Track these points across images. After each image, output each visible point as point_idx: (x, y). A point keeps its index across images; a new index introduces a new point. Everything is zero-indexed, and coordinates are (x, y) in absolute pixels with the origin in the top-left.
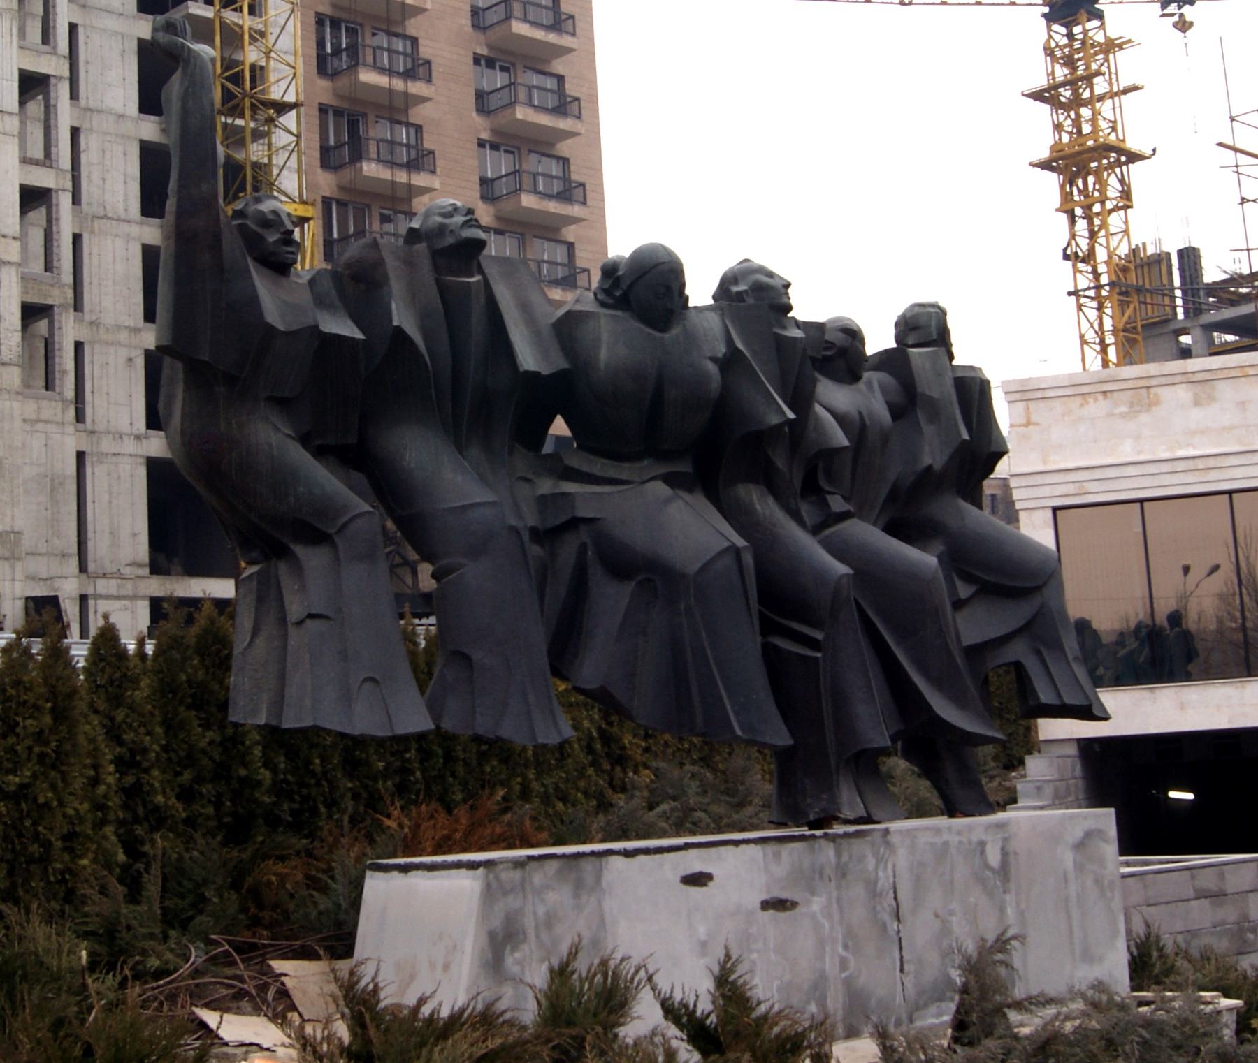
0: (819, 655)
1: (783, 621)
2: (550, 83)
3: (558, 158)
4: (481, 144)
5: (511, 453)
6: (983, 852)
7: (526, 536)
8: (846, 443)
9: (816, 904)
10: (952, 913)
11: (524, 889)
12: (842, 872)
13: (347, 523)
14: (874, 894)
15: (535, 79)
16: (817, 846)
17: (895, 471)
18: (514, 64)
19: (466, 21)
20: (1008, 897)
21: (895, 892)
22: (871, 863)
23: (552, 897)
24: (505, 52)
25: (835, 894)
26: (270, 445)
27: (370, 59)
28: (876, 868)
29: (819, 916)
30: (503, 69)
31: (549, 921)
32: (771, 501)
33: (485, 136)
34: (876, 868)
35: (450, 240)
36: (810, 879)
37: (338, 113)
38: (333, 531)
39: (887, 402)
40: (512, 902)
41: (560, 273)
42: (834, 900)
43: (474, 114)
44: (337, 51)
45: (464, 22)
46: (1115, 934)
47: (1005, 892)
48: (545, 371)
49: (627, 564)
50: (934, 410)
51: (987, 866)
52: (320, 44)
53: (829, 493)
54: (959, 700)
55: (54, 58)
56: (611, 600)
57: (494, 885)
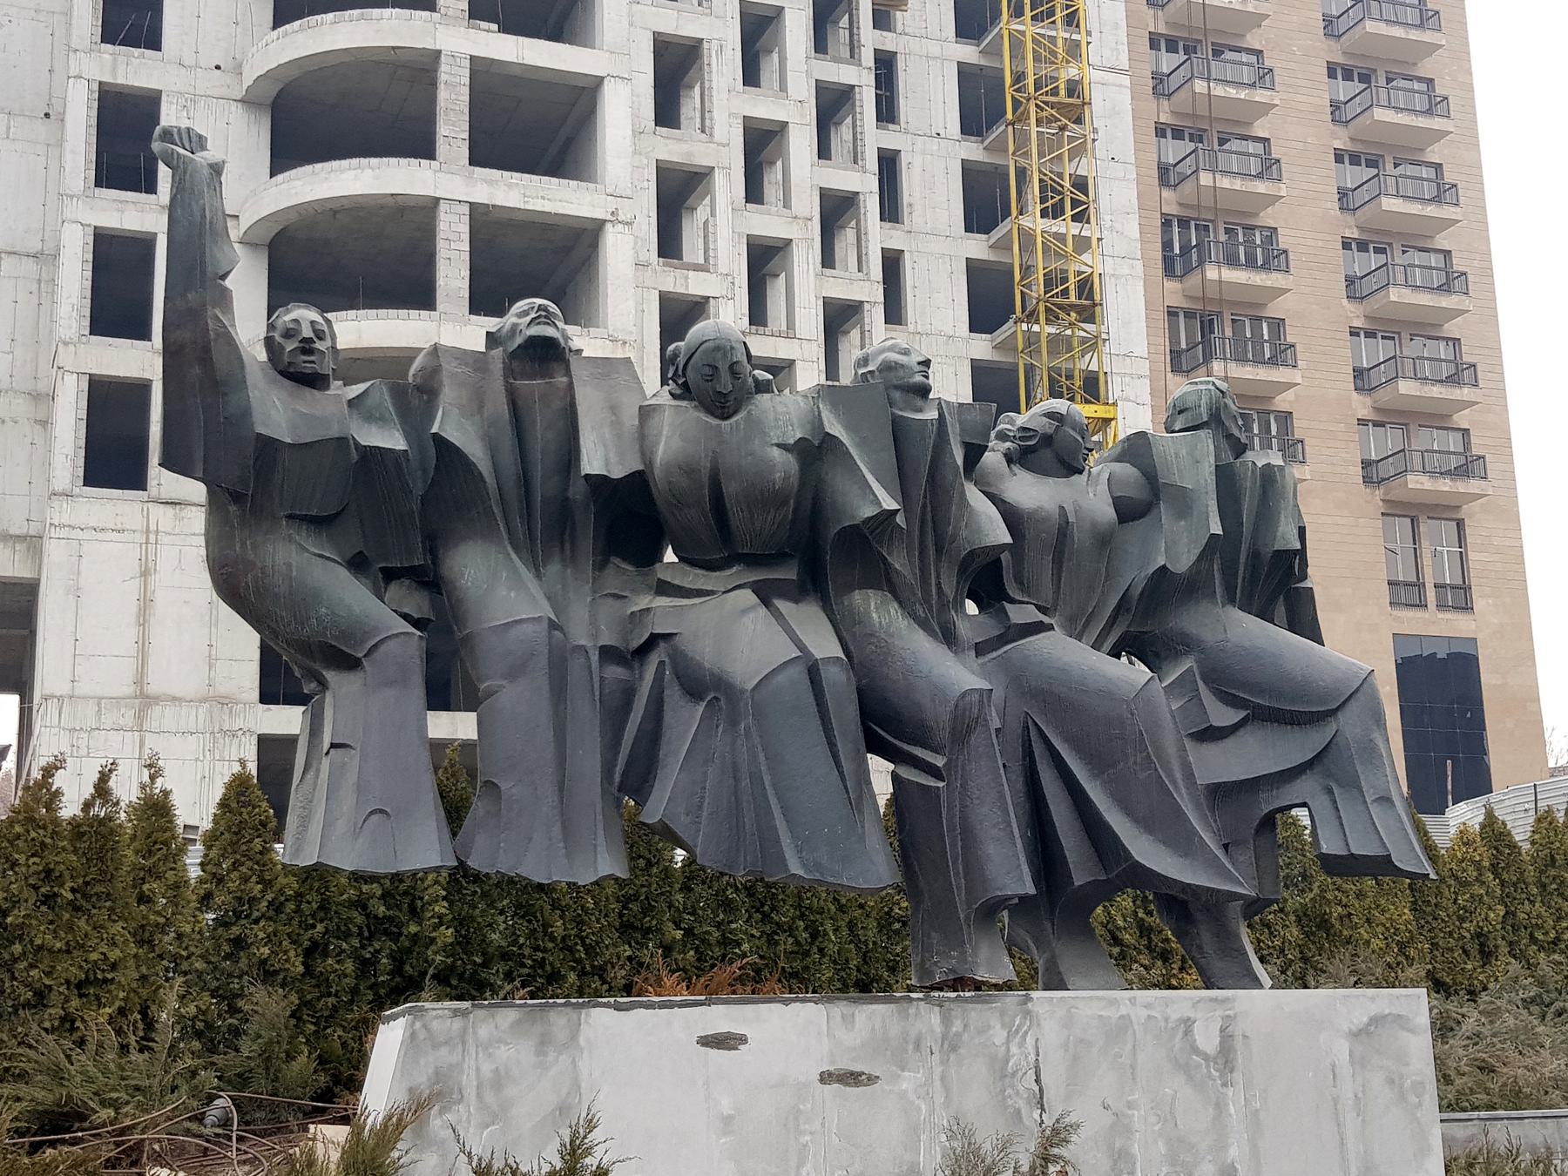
0: (941, 784)
1: (906, 747)
2: (1435, 260)
3: (1447, 339)
4: (1354, 333)
5: (601, 566)
6: (1188, 1032)
7: (595, 657)
8: (1008, 539)
9: (909, 1082)
10: (1130, 1105)
11: (464, 1043)
12: (951, 1045)
13: (376, 646)
14: (1002, 1072)
15: (1417, 258)
16: (912, 1011)
17: (1134, 574)
18: (1390, 245)
19: (1333, 204)
20: (1230, 1092)
21: (1038, 1074)
22: (999, 1035)
23: (503, 1053)
24: (1377, 232)
25: (938, 1070)
26: (289, 565)
27: (1400, 278)
28: (1008, 1042)
29: (912, 1097)
30: (1377, 250)
31: (499, 1081)
32: (894, 607)
33: (1357, 323)
34: (1008, 1042)
35: (519, 340)
36: (903, 1052)
37: (1189, 315)
38: (360, 655)
39: (1114, 499)
40: (445, 1056)
41: (1454, 462)
42: (936, 1077)
43: (1345, 301)
44: (1186, 249)
45: (1329, 205)
46: (1424, 1151)
47: (1224, 1085)
48: (617, 473)
49: (700, 685)
50: (1184, 502)
51: (1195, 1050)
52: (1167, 245)
53: (1013, 601)
54: (1181, 840)
55: (867, 284)
56: (685, 721)
57: (422, 1035)
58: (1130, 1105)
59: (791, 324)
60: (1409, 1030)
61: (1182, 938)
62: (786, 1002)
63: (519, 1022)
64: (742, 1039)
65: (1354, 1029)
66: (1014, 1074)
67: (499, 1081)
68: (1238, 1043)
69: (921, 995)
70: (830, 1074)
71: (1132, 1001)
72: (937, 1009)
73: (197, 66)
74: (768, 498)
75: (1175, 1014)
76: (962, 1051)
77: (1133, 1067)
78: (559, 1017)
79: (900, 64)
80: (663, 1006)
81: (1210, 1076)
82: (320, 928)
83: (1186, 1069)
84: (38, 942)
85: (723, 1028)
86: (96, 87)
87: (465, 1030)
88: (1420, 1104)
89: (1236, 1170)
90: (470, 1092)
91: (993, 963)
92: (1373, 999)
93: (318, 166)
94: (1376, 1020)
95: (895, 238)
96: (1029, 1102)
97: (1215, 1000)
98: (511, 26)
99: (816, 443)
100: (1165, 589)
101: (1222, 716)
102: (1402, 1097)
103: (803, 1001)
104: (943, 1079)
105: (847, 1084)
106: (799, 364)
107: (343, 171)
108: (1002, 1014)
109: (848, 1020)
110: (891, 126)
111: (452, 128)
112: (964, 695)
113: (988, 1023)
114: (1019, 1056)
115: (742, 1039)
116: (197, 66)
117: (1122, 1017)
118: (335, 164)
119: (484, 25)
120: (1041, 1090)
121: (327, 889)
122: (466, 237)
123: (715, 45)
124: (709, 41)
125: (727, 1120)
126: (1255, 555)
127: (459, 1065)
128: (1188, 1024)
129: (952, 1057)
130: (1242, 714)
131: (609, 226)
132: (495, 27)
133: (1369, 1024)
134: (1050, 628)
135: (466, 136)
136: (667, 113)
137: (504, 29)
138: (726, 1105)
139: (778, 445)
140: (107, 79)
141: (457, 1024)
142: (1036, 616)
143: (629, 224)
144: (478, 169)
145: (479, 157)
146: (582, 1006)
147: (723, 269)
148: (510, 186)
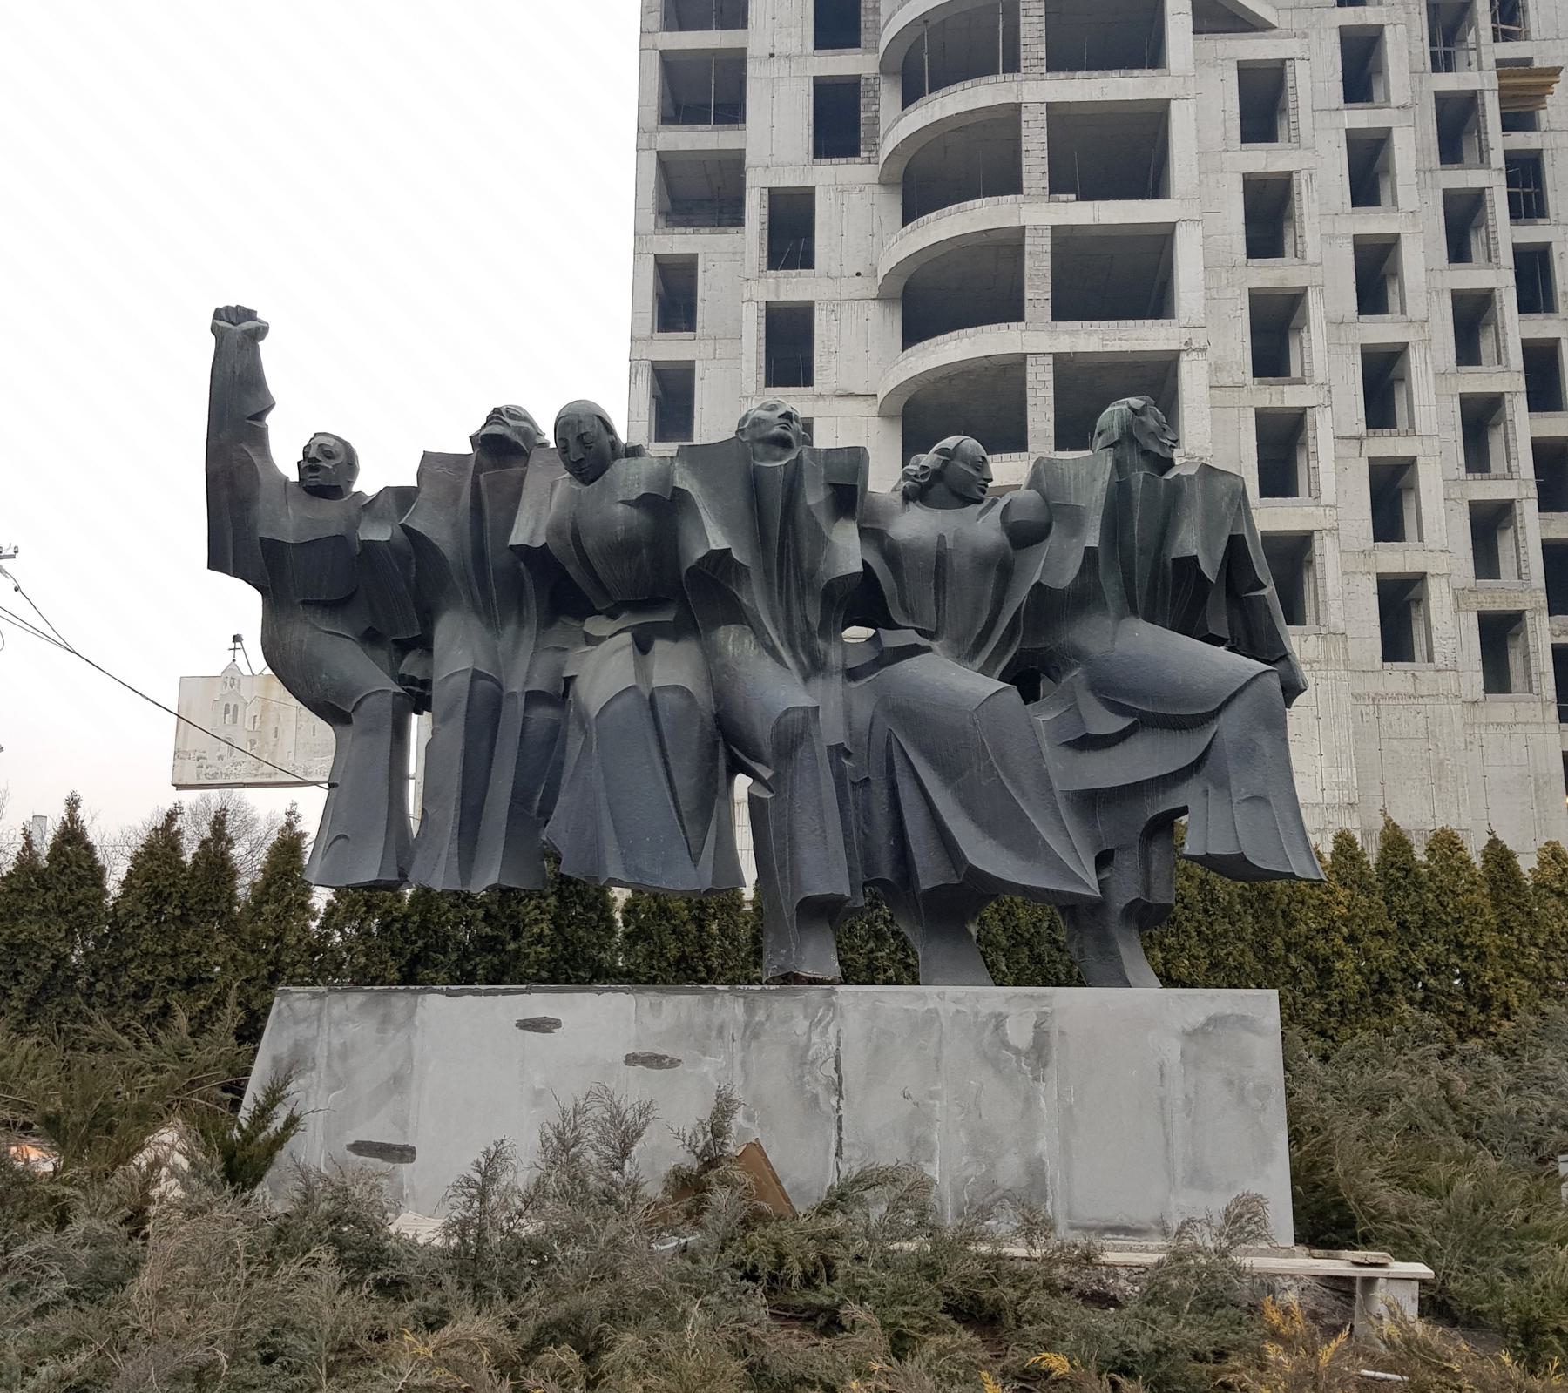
10: (932, 1095)
11: (319, 1020)
12: (753, 1033)
14: (801, 1059)
16: (717, 1001)
20: (1042, 1086)
22: (801, 1025)
23: (351, 1029)
25: (739, 1056)
31: (345, 1053)
34: (810, 1031)
40: (304, 1031)
42: (737, 1063)
47: (1036, 1079)
50: (1074, 518)
51: (1005, 1044)
54: (1026, 843)
57: (286, 1013)
58: (932, 1095)
59: (1412, 425)
60: (1256, 1032)
61: (1044, 944)
62: (599, 992)
63: (363, 1005)
64: (557, 1024)
65: (1189, 1028)
66: (813, 1062)
67: (345, 1053)
68: (1054, 1038)
69: (726, 987)
70: (635, 1057)
71: (941, 996)
72: (741, 1000)
73: (842, 276)
74: (625, 548)
75: (985, 1009)
76: (763, 1039)
77: (937, 1059)
78: (400, 1001)
79: (1547, 160)
80: (487, 993)
81: (1020, 1070)
82: (420, 943)
83: (995, 1063)
84: (144, 947)
85: (540, 1013)
86: (763, 306)
87: (321, 1010)
88: (1264, 1108)
89: (1043, 1163)
90: (322, 1062)
91: (819, 956)
92: (1212, 999)
93: (927, 342)
94: (1216, 1021)
95: (1541, 327)
96: (826, 1086)
97: (1032, 997)
98: (1085, 196)
99: (668, 497)
100: (1048, 607)
101: (1106, 723)
102: (1242, 1098)
103: (615, 991)
104: (743, 1063)
105: (651, 1066)
106: (1420, 462)
107: (945, 343)
108: (806, 1005)
109: (656, 1009)
110: (1540, 221)
111: (1038, 291)
112: (787, 712)
113: (791, 1013)
114: (820, 1045)
115: (557, 1024)
116: (842, 276)
117: (929, 1010)
118: (940, 338)
119: (1063, 197)
120: (840, 1078)
121: (429, 911)
122: (1051, 384)
123: (1304, 176)
124: (1299, 172)
125: (538, 1094)
126: (1158, 563)
127: (314, 1038)
128: (999, 1020)
129: (753, 1044)
130: (1130, 721)
131: (1183, 356)
132: (1073, 197)
133: (1207, 1024)
134: (928, 649)
135: (1049, 296)
136: (1458, 252)
137: (1083, 197)
138: (538, 1080)
139: (623, 502)
140: (772, 298)
141: (315, 1005)
142: (909, 637)
143: (1204, 350)
144: (1059, 324)
145: (1059, 314)
146: (419, 992)
147: (1319, 378)
148: (1090, 334)
